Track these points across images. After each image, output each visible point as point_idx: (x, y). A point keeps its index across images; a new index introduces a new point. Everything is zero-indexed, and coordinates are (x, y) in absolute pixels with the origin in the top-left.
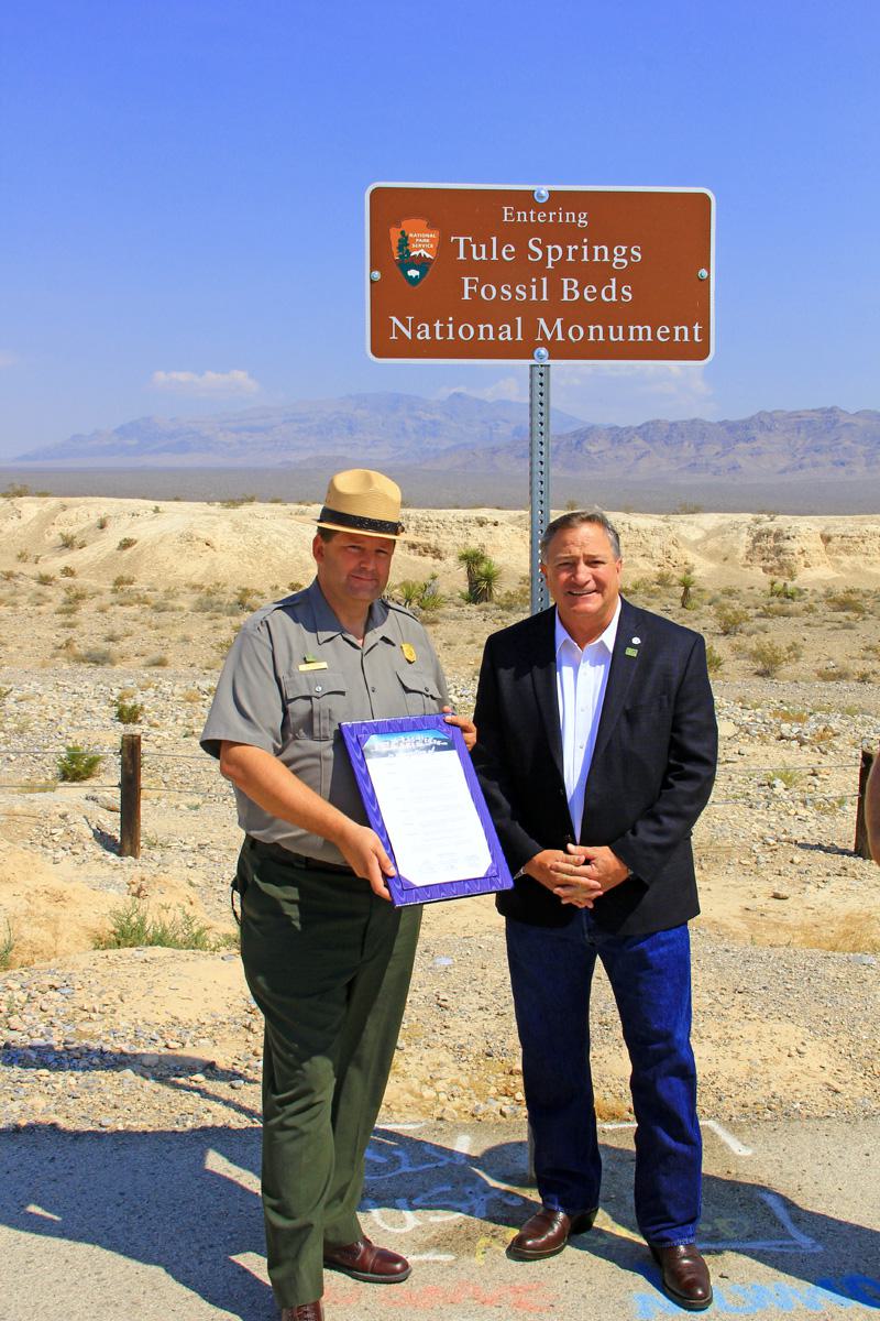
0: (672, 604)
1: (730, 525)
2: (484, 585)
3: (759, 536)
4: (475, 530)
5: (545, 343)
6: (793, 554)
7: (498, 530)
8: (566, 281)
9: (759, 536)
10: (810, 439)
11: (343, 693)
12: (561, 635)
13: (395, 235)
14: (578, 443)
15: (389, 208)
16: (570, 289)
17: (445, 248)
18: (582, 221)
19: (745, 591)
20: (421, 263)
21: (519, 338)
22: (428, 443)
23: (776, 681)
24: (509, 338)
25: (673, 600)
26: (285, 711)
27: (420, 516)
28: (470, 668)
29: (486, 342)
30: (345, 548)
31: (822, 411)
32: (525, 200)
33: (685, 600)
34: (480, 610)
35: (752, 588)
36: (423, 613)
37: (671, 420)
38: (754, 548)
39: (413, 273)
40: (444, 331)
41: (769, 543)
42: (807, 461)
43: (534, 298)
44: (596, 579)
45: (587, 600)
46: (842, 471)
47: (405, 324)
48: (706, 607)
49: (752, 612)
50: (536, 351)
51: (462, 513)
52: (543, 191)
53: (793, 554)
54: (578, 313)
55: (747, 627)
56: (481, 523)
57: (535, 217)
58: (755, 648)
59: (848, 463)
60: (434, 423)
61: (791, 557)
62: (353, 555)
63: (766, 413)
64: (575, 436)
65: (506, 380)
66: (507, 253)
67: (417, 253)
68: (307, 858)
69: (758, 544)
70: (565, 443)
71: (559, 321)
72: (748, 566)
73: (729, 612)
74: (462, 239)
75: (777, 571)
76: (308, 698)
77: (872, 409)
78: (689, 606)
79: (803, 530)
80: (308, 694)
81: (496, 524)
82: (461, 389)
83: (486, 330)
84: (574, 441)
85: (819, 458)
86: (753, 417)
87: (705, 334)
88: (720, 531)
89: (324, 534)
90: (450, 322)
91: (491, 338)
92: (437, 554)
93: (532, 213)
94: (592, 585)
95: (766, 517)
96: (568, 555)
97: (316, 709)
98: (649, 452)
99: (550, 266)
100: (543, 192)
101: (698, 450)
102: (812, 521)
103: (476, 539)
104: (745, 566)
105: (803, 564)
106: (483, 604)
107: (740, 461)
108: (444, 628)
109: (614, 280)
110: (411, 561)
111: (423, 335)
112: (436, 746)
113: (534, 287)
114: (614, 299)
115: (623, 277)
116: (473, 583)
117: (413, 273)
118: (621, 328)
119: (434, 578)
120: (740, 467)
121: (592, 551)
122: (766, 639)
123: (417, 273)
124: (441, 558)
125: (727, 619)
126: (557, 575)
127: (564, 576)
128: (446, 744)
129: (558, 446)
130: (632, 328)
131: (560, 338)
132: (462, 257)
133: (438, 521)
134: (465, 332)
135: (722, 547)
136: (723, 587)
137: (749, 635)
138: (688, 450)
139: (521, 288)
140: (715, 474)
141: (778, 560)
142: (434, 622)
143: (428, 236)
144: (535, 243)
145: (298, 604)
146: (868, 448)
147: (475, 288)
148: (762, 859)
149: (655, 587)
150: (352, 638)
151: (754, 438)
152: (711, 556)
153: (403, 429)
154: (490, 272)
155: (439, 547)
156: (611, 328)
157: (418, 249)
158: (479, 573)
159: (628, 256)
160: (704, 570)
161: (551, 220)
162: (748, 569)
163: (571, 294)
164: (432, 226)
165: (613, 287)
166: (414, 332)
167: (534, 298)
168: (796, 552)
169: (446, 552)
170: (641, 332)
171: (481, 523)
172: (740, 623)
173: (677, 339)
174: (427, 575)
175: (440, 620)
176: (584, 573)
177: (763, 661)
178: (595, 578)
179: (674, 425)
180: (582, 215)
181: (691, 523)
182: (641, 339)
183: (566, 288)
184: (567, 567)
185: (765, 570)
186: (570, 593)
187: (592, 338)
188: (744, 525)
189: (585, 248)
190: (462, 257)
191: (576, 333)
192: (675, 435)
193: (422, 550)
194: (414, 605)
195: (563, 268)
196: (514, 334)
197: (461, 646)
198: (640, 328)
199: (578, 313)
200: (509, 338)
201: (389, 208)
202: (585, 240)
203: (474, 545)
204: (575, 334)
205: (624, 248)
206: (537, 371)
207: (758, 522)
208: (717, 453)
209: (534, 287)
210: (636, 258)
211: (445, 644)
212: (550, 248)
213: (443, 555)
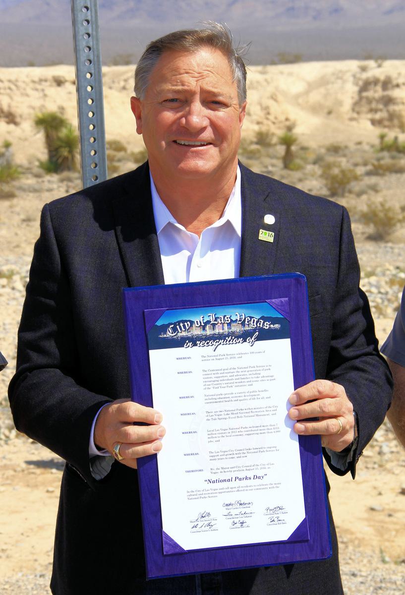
0: (273, 165)
1: (333, 74)
2: (65, 152)
3: (366, 86)
9: (366, 86)
12: (162, 215)
19: (352, 146)
23: (390, 245)
25: (274, 161)
33: (288, 160)
34: (62, 181)
35: (359, 143)
38: (361, 98)
41: (377, 92)
44: (213, 124)
45: (198, 155)
48: (309, 168)
49: (360, 170)
51: (37, 72)
55: (356, 186)
58: (365, 209)
69: (365, 94)
73: (336, 171)
75: (386, 123)
78: (292, 166)
88: (323, 82)
94: (208, 134)
95: (372, 63)
96: (180, 88)
104: (352, 119)
106: (66, 174)
112: (261, 330)
121: (212, 83)
122: (378, 199)
125: (334, 179)
128: (277, 326)
133: (10, 81)
136: (328, 142)
137: (359, 194)
140: (315, 18)
141: (388, 111)
148: (385, 449)
149: (254, 147)
152: (315, 109)
155: (13, 110)
158: (59, 139)
160: (308, 127)
162: (354, 123)
175: (17, 193)
176: (199, 115)
177: (375, 224)
178: (213, 124)
181: (290, 74)
184: (175, 104)
185: (373, 122)
186: (175, 142)
203: (52, 107)
207: (364, 69)
213: (18, 120)
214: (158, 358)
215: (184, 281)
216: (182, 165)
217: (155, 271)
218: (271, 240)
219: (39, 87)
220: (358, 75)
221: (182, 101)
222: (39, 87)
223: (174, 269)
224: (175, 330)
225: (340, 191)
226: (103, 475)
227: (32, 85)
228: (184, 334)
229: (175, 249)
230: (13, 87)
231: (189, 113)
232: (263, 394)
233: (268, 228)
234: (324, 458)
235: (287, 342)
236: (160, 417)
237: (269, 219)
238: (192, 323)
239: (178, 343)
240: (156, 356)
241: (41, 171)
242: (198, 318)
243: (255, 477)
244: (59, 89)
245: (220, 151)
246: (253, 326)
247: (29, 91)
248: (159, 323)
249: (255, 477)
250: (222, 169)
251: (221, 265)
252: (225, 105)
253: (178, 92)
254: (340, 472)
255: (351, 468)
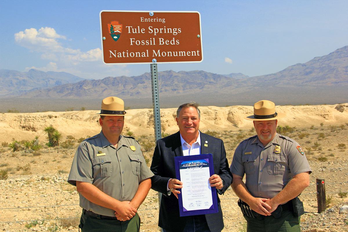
1: (141, 113)
4: (48, 120)
5: (155, 57)
6: (164, 122)
7: (57, 119)
8: (160, 39)
10: (163, 82)
11: (110, 162)
12: (183, 141)
13: (109, 26)
14: (81, 86)
15: (107, 18)
16: (161, 41)
17: (125, 30)
18: (164, 21)
19: (148, 135)
20: (117, 34)
21: (148, 56)
22: (22, 88)
24: (145, 56)
26: (93, 169)
27: (26, 116)
28: (56, 170)
29: (138, 57)
30: (108, 120)
31: (167, 72)
32: (147, 15)
35: (151, 135)
36: (34, 152)
37: (114, 76)
38: (150, 120)
39: (115, 37)
40: (126, 55)
42: (163, 89)
43: (151, 44)
44: (194, 123)
45: (191, 130)
46: (175, 92)
47: (114, 52)
50: (153, 60)
51: (43, 114)
52: (152, 12)
53: (164, 122)
54: (164, 48)
56: (50, 117)
57: (150, 20)
59: (177, 89)
60: (24, 80)
61: (163, 123)
62: (112, 123)
63: (147, 73)
64: (79, 84)
65: (144, 68)
66: (143, 31)
67: (116, 31)
68: (101, 215)
69: (151, 119)
70: (75, 86)
71: (159, 51)
72: (148, 127)
74: (129, 27)
76: (99, 165)
77: (183, 70)
79: (166, 113)
80: (99, 163)
81: (56, 117)
82: (33, 68)
83: (138, 54)
84: (79, 86)
85: (167, 88)
86: (143, 75)
87: (200, 53)
88: (137, 115)
89: (102, 117)
90: (127, 52)
91: (140, 56)
92: (34, 129)
93: (149, 19)
94: (192, 125)
97: (102, 167)
98: (106, 89)
99: (155, 35)
100: (152, 13)
101: (124, 87)
102: (169, 110)
103: (49, 123)
105: (168, 125)
106: (56, 147)
107: (140, 90)
108: (43, 156)
109: (174, 38)
110: (24, 133)
111: (119, 56)
112: (203, 165)
113: (151, 41)
114: (174, 44)
115: (176, 37)
116: (51, 138)
117: (115, 37)
118: (177, 52)
119: (37, 138)
120: (140, 93)
121: (193, 115)
123: (117, 37)
124: (35, 131)
125: (146, 146)
126: (182, 122)
127: (184, 122)
129: (73, 88)
130: (180, 52)
131: (159, 56)
132: (129, 32)
133: (33, 117)
134: (132, 55)
135: (139, 121)
138: (121, 87)
139: (147, 41)
140: (131, 95)
142: (39, 154)
143: (119, 26)
144: (151, 28)
145: (96, 138)
146: (183, 84)
147: (134, 41)
150: (113, 146)
151: (144, 82)
152: (135, 124)
153: (11, 83)
154: (138, 37)
155: (34, 127)
156: (174, 52)
157: (116, 30)
159: (177, 31)
161: (155, 21)
162: (148, 128)
163: (162, 43)
164: (120, 24)
165: (174, 40)
166: (117, 55)
167: (151, 44)
168: (165, 121)
169: (37, 129)
170: (182, 53)
171: (50, 117)
172: (151, 147)
173: (193, 55)
174: (35, 137)
175: (41, 153)
176: (191, 122)
179: (115, 78)
180: (163, 20)
182: (182, 55)
183: (160, 41)
186: (185, 127)
187: (168, 56)
188: (146, 113)
189: (165, 29)
190: (129, 32)
191: (164, 54)
192: (116, 82)
193: (27, 128)
194: (30, 149)
195: (159, 35)
196: (146, 55)
197: (51, 163)
198: (182, 52)
199: (164, 48)
200: (145, 56)
201: (107, 18)
202: (165, 27)
204: (164, 54)
205: (176, 29)
206: (153, 66)
208: (131, 88)
209: (151, 41)
210: (179, 32)
211: (45, 162)
212: (155, 29)
213: (36, 130)
214: (181, 171)
215: (188, 155)
216: (187, 132)
217: (181, 153)
218: (207, 146)
219: (43, 119)
220: (149, 113)
221: (187, 118)
222: (43, 119)
223: (185, 153)
224: (185, 165)
225: (149, 150)
226: (283, 142)
227: (41, 118)
228: (187, 166)
229: (186, 149)
230: (34, 119)
231: (188, 121)
232: (204, 179)
233: (207, 144)
234: (216, 192)
235: (208, 168)
236: (182, 184)
237: (206, 142)
238: (189, 164)
239: (186, 168)
240: (181, 170)
241: (47, 146)
242: (190, 163)
243: (202, 196)
244: (50, 119)
245: (195, 129)
246: (201, 164)
247: (40, 120)
248: (182, 164)
249: (202, 196)
250: (196, 132)
251: (196, 152)
252: (196, 119)
253: (186, 117)
254: (221, 194)
255: (223, 193)
